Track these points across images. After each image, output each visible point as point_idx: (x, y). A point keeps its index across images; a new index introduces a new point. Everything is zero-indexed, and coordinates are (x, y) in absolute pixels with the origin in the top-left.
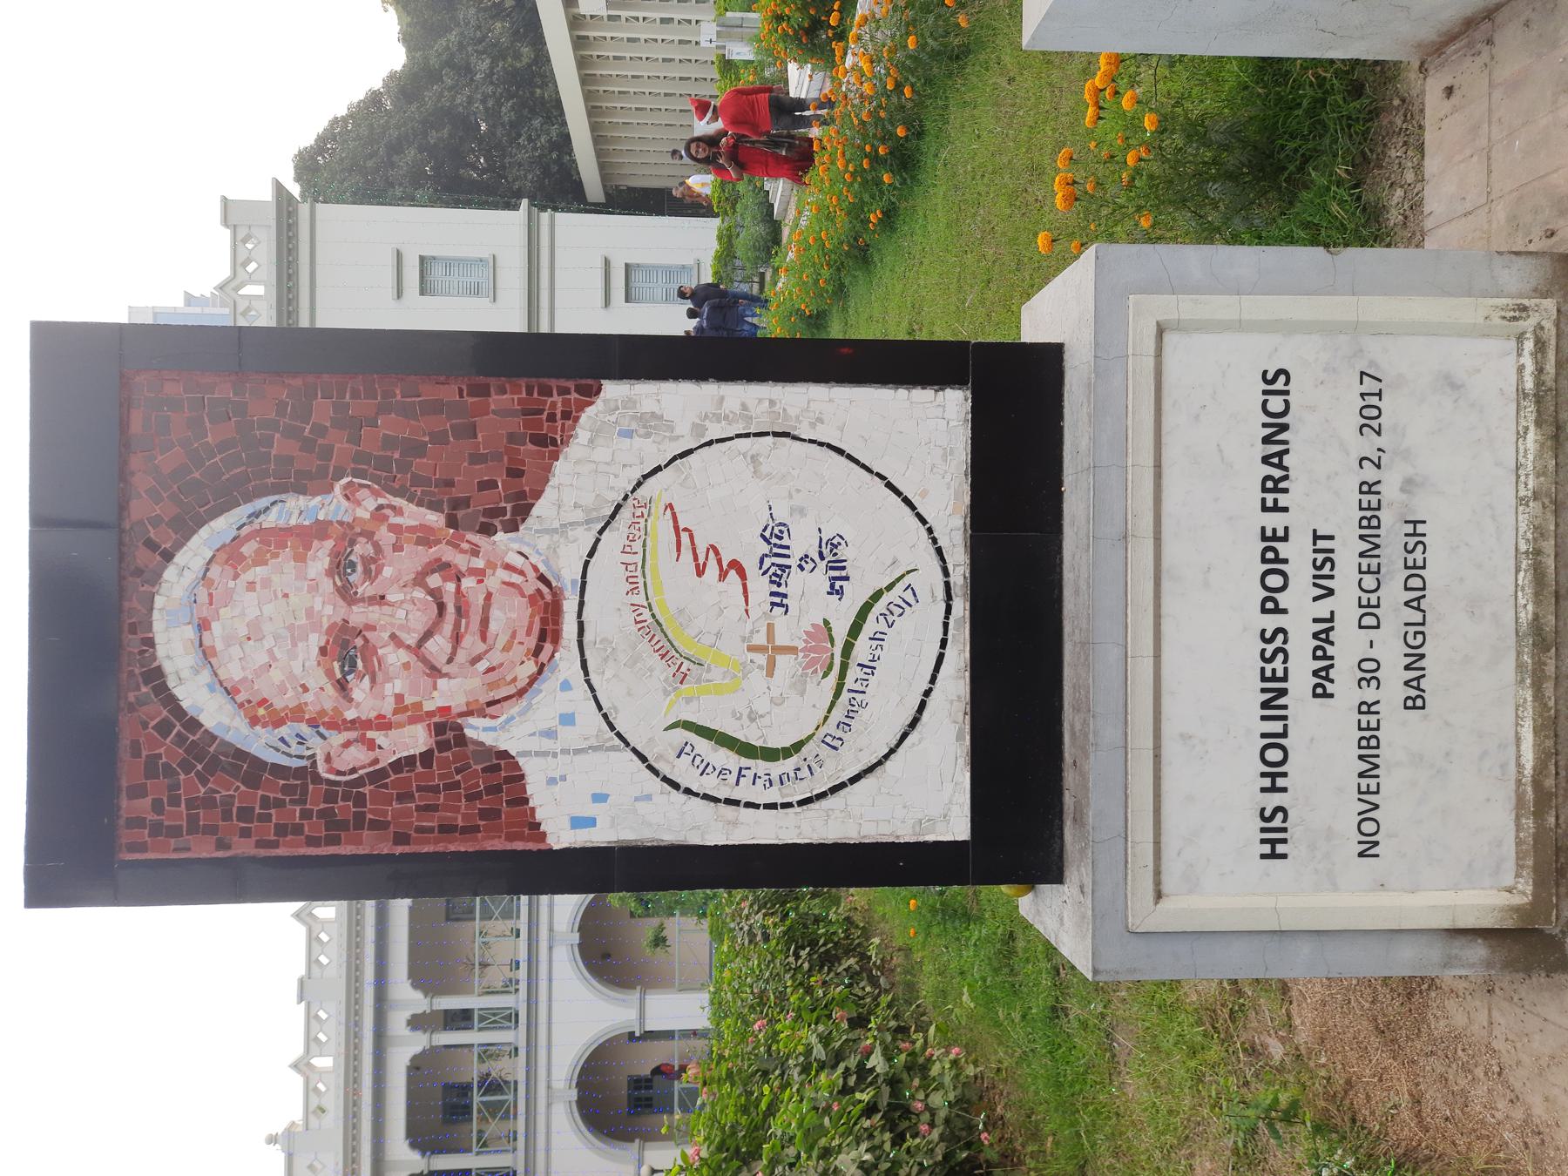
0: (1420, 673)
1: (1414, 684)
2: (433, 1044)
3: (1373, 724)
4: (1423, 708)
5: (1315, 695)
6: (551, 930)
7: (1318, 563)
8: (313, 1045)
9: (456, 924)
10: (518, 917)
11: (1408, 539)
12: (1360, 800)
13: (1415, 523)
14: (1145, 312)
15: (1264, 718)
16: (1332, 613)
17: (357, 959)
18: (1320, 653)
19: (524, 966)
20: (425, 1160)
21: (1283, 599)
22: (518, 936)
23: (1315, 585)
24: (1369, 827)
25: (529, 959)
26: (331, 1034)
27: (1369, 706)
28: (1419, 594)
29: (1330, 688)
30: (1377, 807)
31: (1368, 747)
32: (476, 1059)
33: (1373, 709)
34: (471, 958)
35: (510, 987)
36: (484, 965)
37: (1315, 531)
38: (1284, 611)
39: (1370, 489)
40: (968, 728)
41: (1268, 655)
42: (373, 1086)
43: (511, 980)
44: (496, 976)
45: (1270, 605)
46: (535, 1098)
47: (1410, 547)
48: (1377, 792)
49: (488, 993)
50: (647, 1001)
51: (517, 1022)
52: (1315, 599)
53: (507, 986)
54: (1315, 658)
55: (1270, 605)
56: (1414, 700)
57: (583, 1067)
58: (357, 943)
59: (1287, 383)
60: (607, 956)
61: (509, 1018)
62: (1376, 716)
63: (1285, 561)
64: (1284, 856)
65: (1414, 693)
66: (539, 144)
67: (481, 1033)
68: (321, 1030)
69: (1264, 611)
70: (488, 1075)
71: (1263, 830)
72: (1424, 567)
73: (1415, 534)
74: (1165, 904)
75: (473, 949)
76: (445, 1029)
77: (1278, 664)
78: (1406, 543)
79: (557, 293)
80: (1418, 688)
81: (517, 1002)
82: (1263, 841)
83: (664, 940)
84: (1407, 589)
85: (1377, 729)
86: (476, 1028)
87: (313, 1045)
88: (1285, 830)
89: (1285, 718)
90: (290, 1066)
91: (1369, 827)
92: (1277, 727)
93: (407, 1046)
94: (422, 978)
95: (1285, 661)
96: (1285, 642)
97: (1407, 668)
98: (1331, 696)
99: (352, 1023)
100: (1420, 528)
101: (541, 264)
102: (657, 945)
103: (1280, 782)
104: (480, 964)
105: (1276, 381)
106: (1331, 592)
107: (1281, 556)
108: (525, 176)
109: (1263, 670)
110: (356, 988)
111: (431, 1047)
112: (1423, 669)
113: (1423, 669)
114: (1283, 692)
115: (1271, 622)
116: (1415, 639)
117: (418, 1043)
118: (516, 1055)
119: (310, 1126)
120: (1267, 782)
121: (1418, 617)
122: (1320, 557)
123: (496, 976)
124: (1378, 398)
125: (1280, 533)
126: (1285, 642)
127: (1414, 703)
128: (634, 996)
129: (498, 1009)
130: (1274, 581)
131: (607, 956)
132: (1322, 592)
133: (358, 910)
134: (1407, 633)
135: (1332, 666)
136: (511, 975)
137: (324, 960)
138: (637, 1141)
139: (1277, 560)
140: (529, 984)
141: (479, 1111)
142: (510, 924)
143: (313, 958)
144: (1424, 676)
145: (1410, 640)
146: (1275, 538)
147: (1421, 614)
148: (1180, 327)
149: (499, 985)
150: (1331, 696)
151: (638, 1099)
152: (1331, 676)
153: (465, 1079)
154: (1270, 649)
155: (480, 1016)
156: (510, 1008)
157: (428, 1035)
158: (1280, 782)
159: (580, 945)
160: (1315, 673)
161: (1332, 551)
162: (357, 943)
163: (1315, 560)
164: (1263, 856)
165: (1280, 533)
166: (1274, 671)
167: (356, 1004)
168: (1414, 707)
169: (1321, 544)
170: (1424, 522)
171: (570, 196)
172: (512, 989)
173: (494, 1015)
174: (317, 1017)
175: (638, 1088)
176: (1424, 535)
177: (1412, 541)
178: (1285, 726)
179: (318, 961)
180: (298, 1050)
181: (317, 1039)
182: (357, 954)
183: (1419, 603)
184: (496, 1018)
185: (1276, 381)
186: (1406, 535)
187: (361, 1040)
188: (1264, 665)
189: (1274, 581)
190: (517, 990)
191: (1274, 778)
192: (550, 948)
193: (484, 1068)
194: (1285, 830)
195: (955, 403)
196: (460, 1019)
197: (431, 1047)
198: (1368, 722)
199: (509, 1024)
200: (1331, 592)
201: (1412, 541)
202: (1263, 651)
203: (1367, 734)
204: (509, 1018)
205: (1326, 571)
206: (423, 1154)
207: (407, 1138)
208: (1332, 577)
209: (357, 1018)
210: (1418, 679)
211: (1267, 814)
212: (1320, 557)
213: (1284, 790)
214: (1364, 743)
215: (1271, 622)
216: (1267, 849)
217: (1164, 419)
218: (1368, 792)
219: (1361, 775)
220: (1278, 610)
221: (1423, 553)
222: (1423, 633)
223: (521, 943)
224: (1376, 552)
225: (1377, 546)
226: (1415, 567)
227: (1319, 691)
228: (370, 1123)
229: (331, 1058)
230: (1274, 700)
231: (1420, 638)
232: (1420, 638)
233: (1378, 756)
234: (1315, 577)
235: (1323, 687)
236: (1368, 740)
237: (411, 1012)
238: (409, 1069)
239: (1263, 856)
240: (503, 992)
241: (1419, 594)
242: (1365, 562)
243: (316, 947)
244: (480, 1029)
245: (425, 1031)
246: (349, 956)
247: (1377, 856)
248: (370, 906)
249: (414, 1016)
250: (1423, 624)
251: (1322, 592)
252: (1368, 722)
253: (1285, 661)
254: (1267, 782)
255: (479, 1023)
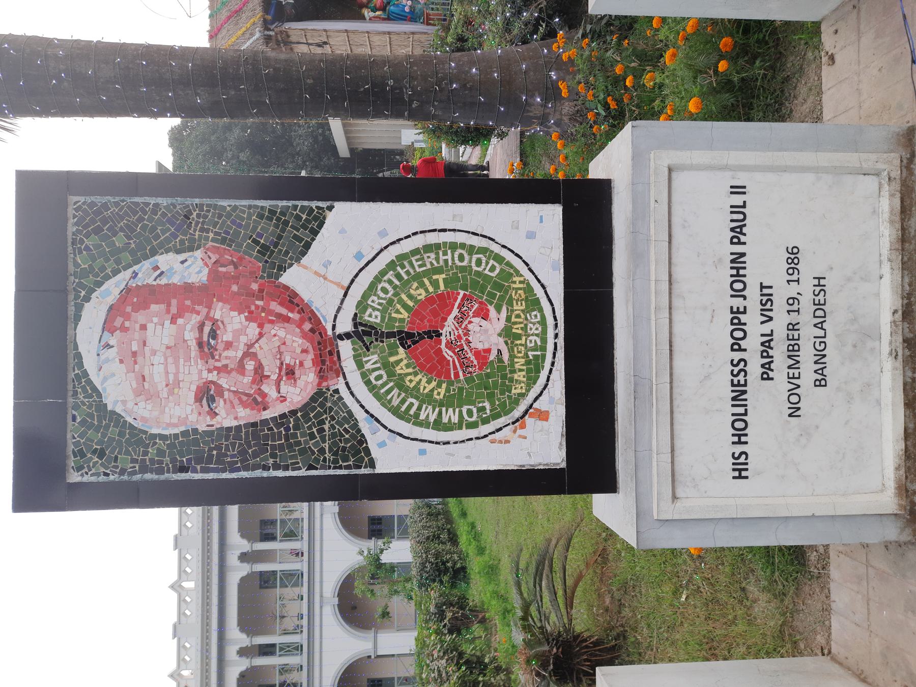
0: (824, 365)
1: (820, 372)
2: (253, 665)
3: (796, 337)
4: (825, 385)
5: (763, 379)
6: (321, 596)
7: (764, 302)
8: (183, 575)
9: (265, 590)
10: (302, 585)
11: (815, 288)
12: (789, 382)
13: (819, 279)
14: (662, 159)
15: (733, 406)
16: (772, 331)
17: (207, 612)
18: (765, 354)
19: (305, 618)
20: (250, 638)
21: (743, 344)
22: (302, 599)
23: (762, 315)
24: (794, 399)
25: (309, 528)
26: (194, 568)
27: (793, 326)
28: (822, 319)
29: (771, 374)
30: (799, 386)
31: (793, 350)
32: (278, 671)
33: (796, 327)
34: (275, 613)
35: (297, 630)
36: (282, 617)
37: (761, 283)
38: (745, 350)
39: (793, 327)
40: (564, 443)
41: (735, 373)
42: (218, 616)
43: (298, 626)
44: (289, 624)
45: (736, 347)
46: (313, 615)
47: (816, 293)
48: (799, 378)
49: (285, 633)
50: (378, 638)
51: (302, 650)
52: (762, 323)
53: (296, 629)
54: (762, 357)
55: (736, 347)
56: (820, 381)
57: (341, 677)
58: (208, 569)
59: (746, 459)
60: (354, 608)
61: (297, 649)
62: (798, 332)
63: (745, 324)
64: (746, 477)
65: (820, 377)
66: (311, 125)
67: (280, 658)
68: (188, 566)
69: (733, 350)
70: (285, 682)
71: (734, 464)
72: (824, 304)
73: (819, 285)
74: (678, 504)
75: (275, 607)
76: (259, 656)
77: (741, 377)
78: (814, 290)
79: (324, 668)
80: (822, 374)
81: (302, 639)
82: (734, 470)
83: (388, 613)
84: (815, 317)
85: (798, 340)
86: (278, 540)
87: (182, 663)
88: (747, 464)
89: (746, 405)
90: (168, 676)
91: (794, 399)
92: (741, 410)
93: (238, 571)
94: (245, 625)
95: (745, 376)
96: (745, 366)
97: (816, 362)
98: (772, 379)
99: (205, 677)
100: (822, 282)
101: (315, 570)
102: (384, 617)
103: (743, 439)
104: (280, 617)
105: (740, 472)
106: (771, 319)
107: (742, 322)
108: (303, 142)
109: (732, 380)
110: (207, 623)
111: (252, 645)
112: (825, 363)
113: (825, 363)
114: (745, 392)
115: (737, 356)
116: (820, 345)
117: (243, 664)
118: (301, 670)
119: (182, 534)
120: (736, 439)
121: (821, 333)
122: (765, 299)
123: (289, 624)
124: (797, 283)
125: (742, 310)
126: (745, 366)
127: (820, 383)
128: (370, 634)
129: (290, 643)
130: (738, 334)
131: (354, 608)
132: (766, 319)
133: (208, 510)
134: (815, 342)
135: (772, 362)
136: (297, 623)
137: (189, 524)
138: (373, 538)
139: (740, 323)
140: (309, 629)
141: (281, 578)
142: (297, 590)
143: (182, 612)
144: (825, 367)
145: (817, 346)
146: (738, 312)
147: (824, 331)
148: (683, 168)
149: (291, 629)
150: (772, 379)
151: (374, 531)
152: (772, 345)
153: (273, 683)
154: (736, 370)
155: (280, 647)
156: (298, 643)
157: (249, 660)
158: (743, 439)
159: (339, 513)
160: (763, 366)
161: (771, 295)
162: (208, 583)
163: (762, 300)
164: (734, 478)
165: (742, 310)
166: (739, 381)
167: (208, 552)
168: (820, 385)
169: (765, 291)
170: (824, 278)
171: (330, 153)
172: (299, 631)
173: (289, 647)
174: (184, 647)
175: (373, 524)
176: (824, 286)
177: (818, 289)
178: (746, 410)
179: (185, 558)
180: (174, 577)
181: (184, 660)
182: (207, 609)
183: (822, 325)
184: (289, 649)
185: (740, 472)
186: (814, 286)
187: (210, 660)
188: (733, 378)
189: (738, 334)
190: (302, 631)
191: (740, 437)
192: (321, 607)
193: (283, 678)
194: (747, 464)
195: (553, 214)
196: (267, 650)
197: (252, 645)
198: (794, 373)
199: (297, 652)
200: (771, 319)
201: (818, 289)
202: (732, 371)
203: (793, 342)
204: (297, 649)
205: (768, 306)
206: (249, 541)
207: (239, 532)
208: (771, 310)
209: (208, 641)
210: (822, 369)
211: (736, 455)
212: (765, 299)
213: (746, 443)
214: (791, 348)
215: (737, 356)
216: (736, 474)
217: (675, 459)
218: (794, 378)
219: (789, 367)
220: (740, 349)
221: (824, 296)
222: (825, 342)
223: (304, 604)
224: (796, 366)
225: (798, 362)
226: (819, 304)
227: (765, 376)
228: (217, 620)
229: (194, 582)
230: (739, 394)
231: (823, 345)
232: (823, 345)
233: (799, 356)
234: (762, 310)
235: (767, 374)
236: (793, 346)
237: (240, 552)
238: (238, 680)
239: (734, 478)
240: (293, 633)
241: (822, 319)
242: (791, 371)
243: (183, 605)
244: (280, 656)
245: (248, 657)
246: (203, 611)
247: (800, 416)
248: (215, 510)
249: (241, 649)
250: (825, 337)
251: (766, 319)
252: (794, 373)
253: (745, 376)
254: (736, 439)
255: (280, 651)
